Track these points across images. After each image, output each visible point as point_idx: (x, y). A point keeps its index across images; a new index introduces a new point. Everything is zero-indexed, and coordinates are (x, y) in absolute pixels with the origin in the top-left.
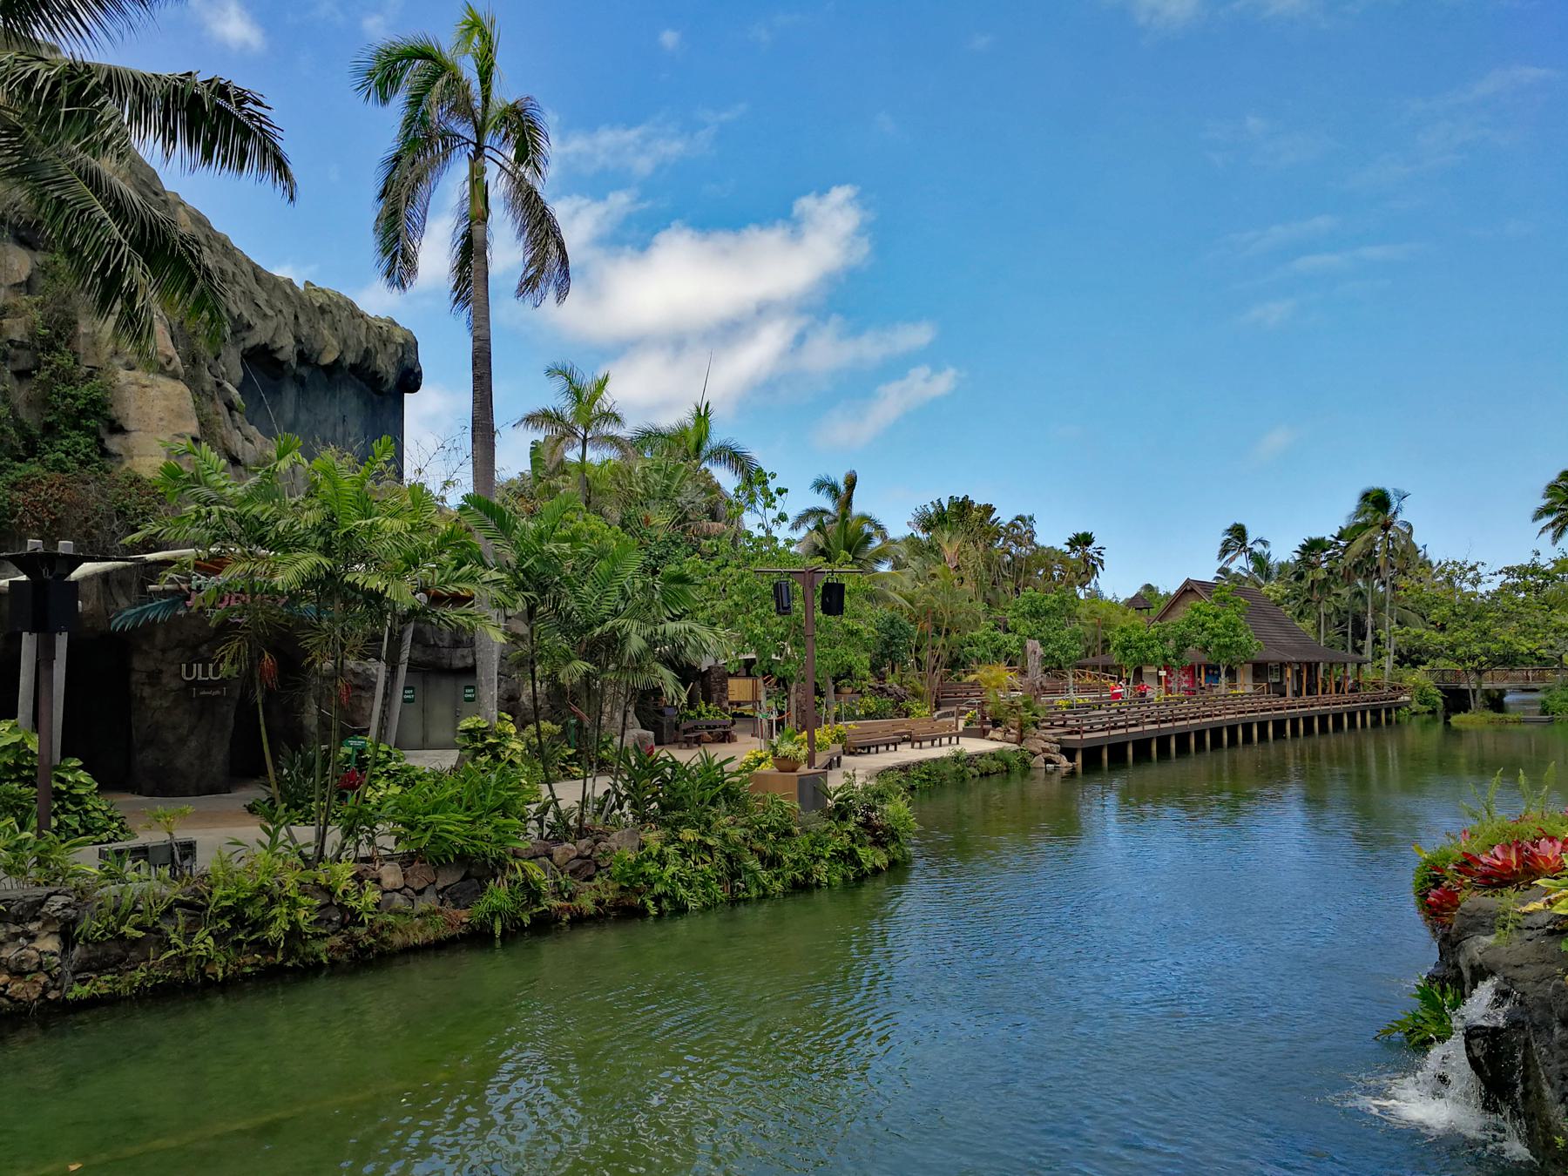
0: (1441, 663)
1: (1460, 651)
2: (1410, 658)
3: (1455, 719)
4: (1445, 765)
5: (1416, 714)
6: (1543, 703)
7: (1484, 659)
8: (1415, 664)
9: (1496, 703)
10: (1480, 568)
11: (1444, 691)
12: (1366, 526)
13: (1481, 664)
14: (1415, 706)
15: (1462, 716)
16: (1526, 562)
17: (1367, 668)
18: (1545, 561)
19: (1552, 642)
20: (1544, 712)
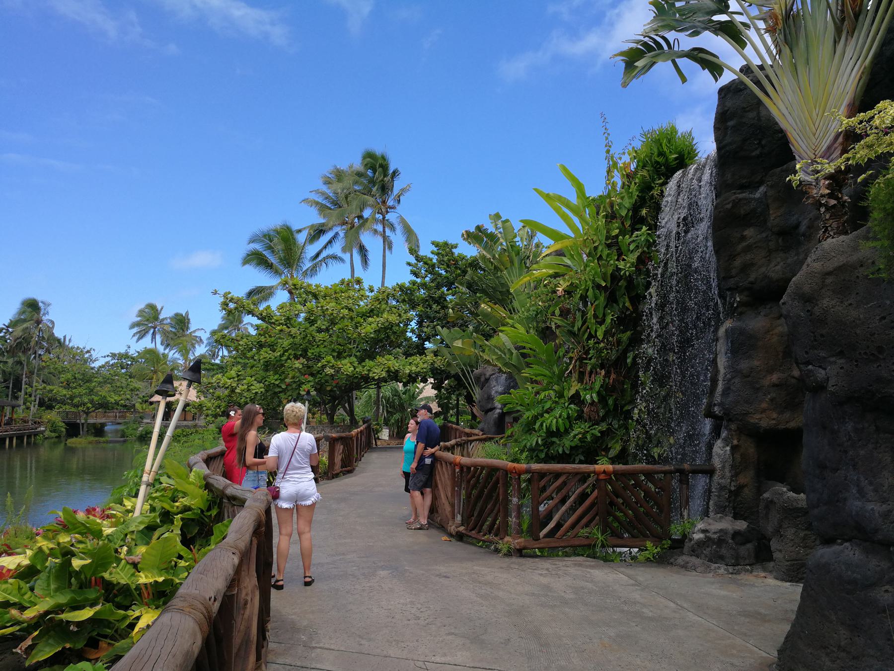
0: (67, 408)
1: (76, 401)
2: (46, 404)
3: (72, 441)
4: (64, 471)
5: (46, 438)
6: (123, 431)
7: (89, 405)
8: (50, 407)
9: (99, 431)
10: (92, 352)
11: (67, 424)
12: (25, 321)
13: (88, 408)
14: (47, 434)
15: (74, 440)
16: (123, 351)
17: (20, 410)
18: (132, 352)
19: (128, 397)
20: (123, 436)
